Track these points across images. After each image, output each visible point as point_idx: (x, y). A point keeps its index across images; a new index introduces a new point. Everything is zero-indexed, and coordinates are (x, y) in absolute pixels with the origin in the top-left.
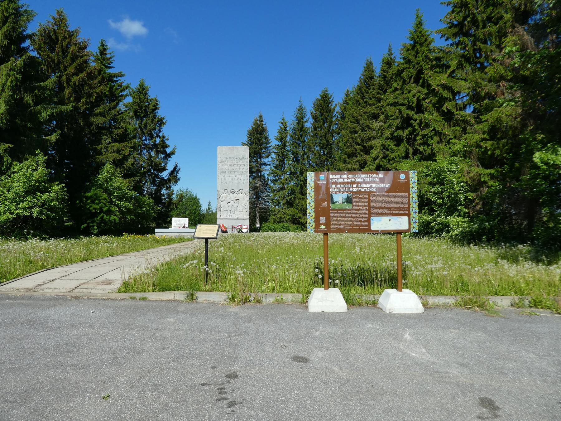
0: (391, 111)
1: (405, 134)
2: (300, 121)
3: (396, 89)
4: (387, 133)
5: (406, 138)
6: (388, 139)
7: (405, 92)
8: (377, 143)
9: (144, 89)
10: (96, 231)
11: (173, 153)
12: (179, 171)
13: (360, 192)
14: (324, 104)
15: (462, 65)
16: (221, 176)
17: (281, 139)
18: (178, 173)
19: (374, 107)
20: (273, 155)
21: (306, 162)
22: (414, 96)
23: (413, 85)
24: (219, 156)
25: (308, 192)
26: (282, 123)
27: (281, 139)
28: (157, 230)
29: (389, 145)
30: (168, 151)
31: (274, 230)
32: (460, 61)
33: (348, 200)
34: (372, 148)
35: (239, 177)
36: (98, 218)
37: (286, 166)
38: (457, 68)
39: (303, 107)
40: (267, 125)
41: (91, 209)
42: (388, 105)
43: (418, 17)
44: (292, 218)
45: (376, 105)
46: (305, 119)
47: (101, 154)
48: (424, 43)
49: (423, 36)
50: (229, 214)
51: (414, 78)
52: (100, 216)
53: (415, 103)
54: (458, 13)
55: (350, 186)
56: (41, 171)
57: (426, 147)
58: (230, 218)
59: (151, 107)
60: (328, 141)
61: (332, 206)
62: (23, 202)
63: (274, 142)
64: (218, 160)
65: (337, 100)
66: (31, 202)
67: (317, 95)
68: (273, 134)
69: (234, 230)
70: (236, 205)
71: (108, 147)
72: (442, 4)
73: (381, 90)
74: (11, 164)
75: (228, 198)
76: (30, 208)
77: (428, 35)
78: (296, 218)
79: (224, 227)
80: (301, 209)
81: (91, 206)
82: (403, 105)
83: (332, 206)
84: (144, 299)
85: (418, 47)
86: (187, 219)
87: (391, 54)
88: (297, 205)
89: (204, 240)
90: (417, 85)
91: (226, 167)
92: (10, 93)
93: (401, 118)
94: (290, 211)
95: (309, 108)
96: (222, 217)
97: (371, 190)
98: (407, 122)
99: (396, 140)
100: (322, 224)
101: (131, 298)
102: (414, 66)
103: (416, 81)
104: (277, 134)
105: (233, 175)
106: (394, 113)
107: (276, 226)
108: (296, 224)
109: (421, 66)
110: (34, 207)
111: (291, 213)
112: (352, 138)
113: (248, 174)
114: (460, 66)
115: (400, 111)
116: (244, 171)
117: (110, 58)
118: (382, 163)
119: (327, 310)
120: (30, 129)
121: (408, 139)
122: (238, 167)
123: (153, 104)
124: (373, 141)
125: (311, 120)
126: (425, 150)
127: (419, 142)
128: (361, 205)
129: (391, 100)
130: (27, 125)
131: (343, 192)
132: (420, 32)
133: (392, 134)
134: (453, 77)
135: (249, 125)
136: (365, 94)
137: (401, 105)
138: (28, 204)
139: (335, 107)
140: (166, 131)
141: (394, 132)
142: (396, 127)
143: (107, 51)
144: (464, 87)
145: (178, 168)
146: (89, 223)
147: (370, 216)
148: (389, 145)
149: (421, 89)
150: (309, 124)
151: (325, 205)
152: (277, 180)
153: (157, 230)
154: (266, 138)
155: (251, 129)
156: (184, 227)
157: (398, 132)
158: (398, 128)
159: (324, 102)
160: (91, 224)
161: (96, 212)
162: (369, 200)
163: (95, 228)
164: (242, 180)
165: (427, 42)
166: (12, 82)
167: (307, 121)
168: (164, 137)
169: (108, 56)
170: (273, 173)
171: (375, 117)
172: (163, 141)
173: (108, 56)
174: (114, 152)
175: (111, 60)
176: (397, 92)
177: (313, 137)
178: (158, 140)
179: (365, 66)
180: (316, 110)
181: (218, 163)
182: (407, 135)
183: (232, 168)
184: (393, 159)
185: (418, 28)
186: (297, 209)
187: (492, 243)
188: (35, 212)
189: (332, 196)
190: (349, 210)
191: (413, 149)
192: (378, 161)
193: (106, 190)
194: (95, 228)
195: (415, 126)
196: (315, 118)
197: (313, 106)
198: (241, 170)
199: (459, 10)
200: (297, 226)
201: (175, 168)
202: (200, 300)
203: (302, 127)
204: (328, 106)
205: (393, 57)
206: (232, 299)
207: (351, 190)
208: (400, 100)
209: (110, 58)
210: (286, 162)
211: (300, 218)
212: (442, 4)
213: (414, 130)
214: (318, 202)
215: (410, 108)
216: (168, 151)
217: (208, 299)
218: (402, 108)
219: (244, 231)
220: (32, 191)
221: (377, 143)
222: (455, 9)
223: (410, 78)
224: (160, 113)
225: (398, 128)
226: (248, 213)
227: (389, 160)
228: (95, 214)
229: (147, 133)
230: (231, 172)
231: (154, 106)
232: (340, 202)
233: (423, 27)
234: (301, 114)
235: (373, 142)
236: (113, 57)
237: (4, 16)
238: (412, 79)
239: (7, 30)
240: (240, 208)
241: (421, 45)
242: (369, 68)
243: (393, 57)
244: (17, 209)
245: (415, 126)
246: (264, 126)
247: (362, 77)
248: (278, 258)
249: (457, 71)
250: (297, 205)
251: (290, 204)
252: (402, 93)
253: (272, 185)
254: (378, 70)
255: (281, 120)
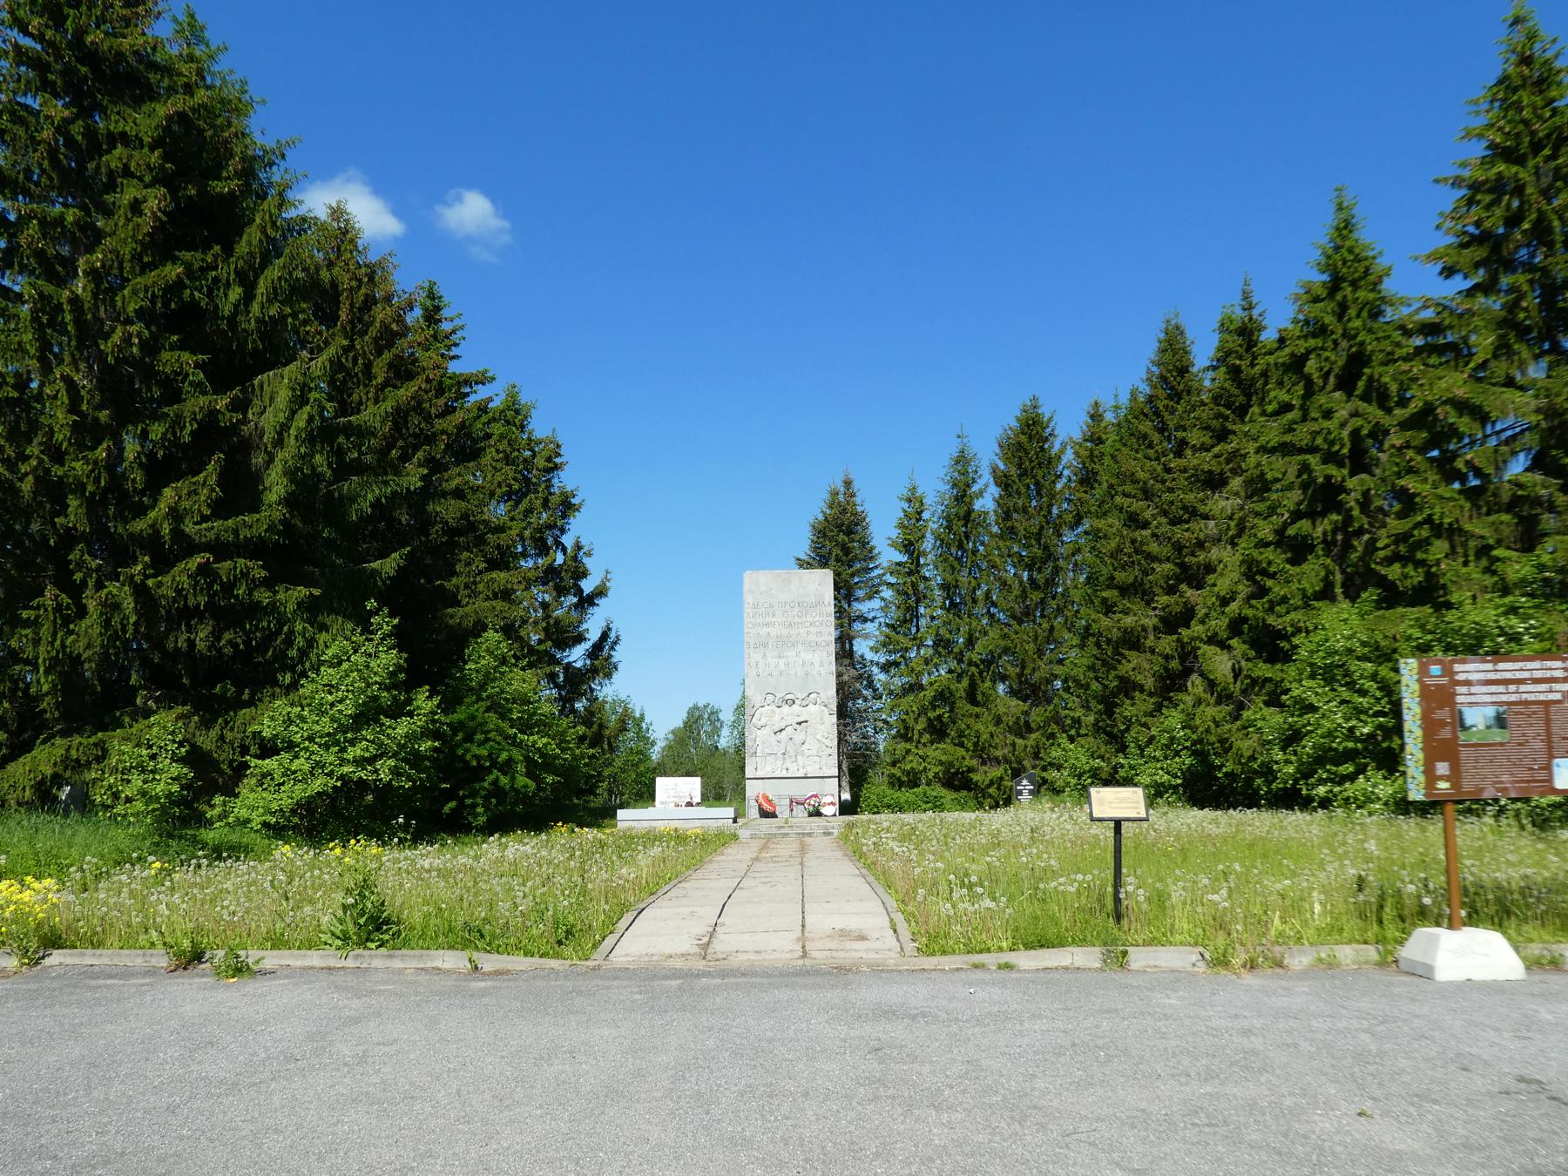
0: (1276, 466)
1: (1320, 529)
2: (962, 494)
3: (1286, 408)
4: (1265, 530)
5: (1324, 541)
6: (1267, 545)
7: (1314, 414)
8: (1228, 559)
9: (517, 412)
10: (482, 820)
11: (601, 592)
12: (615, 643)
13: (1527, 703)
14: (1029, 445)
15: (1508, 346)
16: (756, 656)
17: (909, 546)
18: (612, 648)
19: (1208, 456)
20: (887, 593)
21: (980, 609)
22: (1343, 425)
23: (1337, 394)
24: (749, 599)
25: (1405, 706)
26: (910, 501)
27: (909, 546)
28: (621, 814)
29: (1270, 563)
30: (588, 586)
31: (898, 808)
32: (1500, 337)
33: (1500, 722)
34: (1209, 569)
35: (808, 656)
36: (486, 784)
37: (923, 622)
38: (1495, 357)
39: (970, 453)
40: (867, 507)
41: (468, 757)
42: (1263, 450)
43: (1340, 208)
44: (947, 772)
45: (1216, 450)
46: (975, 488)
47: (458, 603)
48: (1361, 279)
49: (1358, 259)
50: (779, 763)
51: (1337, 376)
52: (491, 778)
53: (1348, 445)
54: (1488, 207)
55: (1501, 689)
56: (388, 659)
57: (1410, 570)
58: (784, 774)
59: (540, 462)
60: (1046, 548)
61: (1462, 736)
62: (352, 743)
63: (887, 555)
64: (748, 610)
65: (1068, 428)
66: (372, 742)
67: (1007, 419)
68: (883, 534)
69: (798, 809)
70: (799, 737)
71: (475, 583)
72: (1437, 181)
73: (1228, 406)
74: (311, 643)
75: (777, 718)
76: (372, 760)
77: (1374, 258)
78: (957, 772)
79: (769, 802)
80: (976, 744)
81: (467, 751)
82: (1312, 450)
83: (1462, 736)
84: (1008, 967)
85: (1348, 290)
86: (698, 780)
87: (1250, 308)
88: (961, 734)
89: (1112, 824)
90: (1350, 395)
91: (770, 629)
92: (303, 450)
93: (1305, 487)
94: (940, 753)
95: (988, 456)
96: (760, 774)
97: (1551, 697)
98: (1325, 497)
99: (1292, 548)
100: (1441, 778)
101: (976, 966)
102: (1335, 342)
103: (1346, 383)
104: (895, 533)
105: (791, 653)
106: (1284, 474)
107: (905, 795)
108: (957, 789)
109: (1362, 344)
110: (380, 756)
111: (944, 758)
112: (1133, 541)
113: (832, 649)
114: (1502, 349)
115: (1305, 468)
116: (819, 639)
117: (454, 332)
118: (1249, 612)
119: (1478, 976)
120: (328, 543)
121: (1328, 544)
122: (803, 631)
123: (545, 454)
124: (1214, 550)
125: (994, 490)
126: (1406, 576)
127: (1382, 554)
128: (1530, 732)
129: (1273, 433)
130: (320, 533)
131: (1485, 704)
132: (1350, 251)
133: (1280, 532)
134: (1479, 380)
135: (815, 509)
136: (1166, 416)
137: (1301, 451)
138: (367, 750)
139: (1063, 450)
140: (577, 530)
141: (1285, 525)
142: (1292, 513)
143: (445, 313)
144: (1516, 411)
145: (613, 635)
146: (465, 797)
147: (1551, 757)
148: (1270, 563)
149: (1362, 406)
150: (987, 501)
151: (1446, 733)
152: (897, 664)
153: (621, 814)
154: (864, 543)
155: (821, 517)
156: (689, 804)
157: (1298, 525)
158: (1297, 516)
159: (1030, 438)
160: (469, 801)
161: (480, 766)
162: (1548, 721)
163: (480, 810)
164: (817, 664)
165: (1371, 278)
166: (311, 419)
167: (981, 494)
168: (578, 547)
169: (446, 327)
170: (885, 644)
171: (1214, 482)
172: (575, 559)
173: (446, 327)
174: (495, 596)
175: (454, 337)
176: (1290, 416)
177: (1001, 537)
178: (560, 559)
179: (1162, 336)
180: (1006, 460)
181: (746, 620)
182: (1325, 533)
183: (785, 632)
184: (1284, 600)
185: (1344, 238)
186: (962, 745)
187: (1383, 835)
188: (384, 770)
189: (1460, 712)
190: (1501, 744)
191: (1343, 572)
192: (1234, 606)
193: (496, 707)
194: (480, 810)
195: (1351, 509)
196: (1003, 481)
197: (998, 450)
198: (812, 638)
199: (1488, 198)
200: (964, 793)
201: (605, 636)
202: (1134, 966)
203: (969, 512)
204: (1042, 448)
205: (1255, 313)
206: (1221, 962)
207: (1504, 698)
208: (1302, 435)
209: (454, 332)
210: (922, 610)
211: (971, 770)
212: (1437, 181)
213: (1348, 519)
214: (1430, 726)
215: (1331, 458)
216: (588, 586)
217: (1152, 963)
218: (1313, 460)
219: (828, 810)
220: (368, 715)
221: (1228, 559)
222: (1479, 197)
223: (1326, 376)
224: (565, 480)
225: (1297, 516)
226: (834, 760)
227: (1270, 601)
228: (479, 772)
229: (532, 537)
230: (783, 643)
231: (549, 459)
232: (1481, 727)
233: (1355, 235)
234: (965, 473)
235: (1215, 553)
236: (462, 328)
237: (267, 236)
238: (1332, 379)
239: (280, 278)
240: (812, 746)
241: (1355, 284)
242: (1173, 349)
243: (1255, 313)
244: (343, 762)
245: (1351, 509)
246: (859, 509)
247: (1154, 369)
248: (1237, 867)
249: (1492, 364)
250: (961, 734)
251: (938, 731)
252: (1304, 419)
253: (882, 677)
254: (1203, 351)
255: (905, 492)
